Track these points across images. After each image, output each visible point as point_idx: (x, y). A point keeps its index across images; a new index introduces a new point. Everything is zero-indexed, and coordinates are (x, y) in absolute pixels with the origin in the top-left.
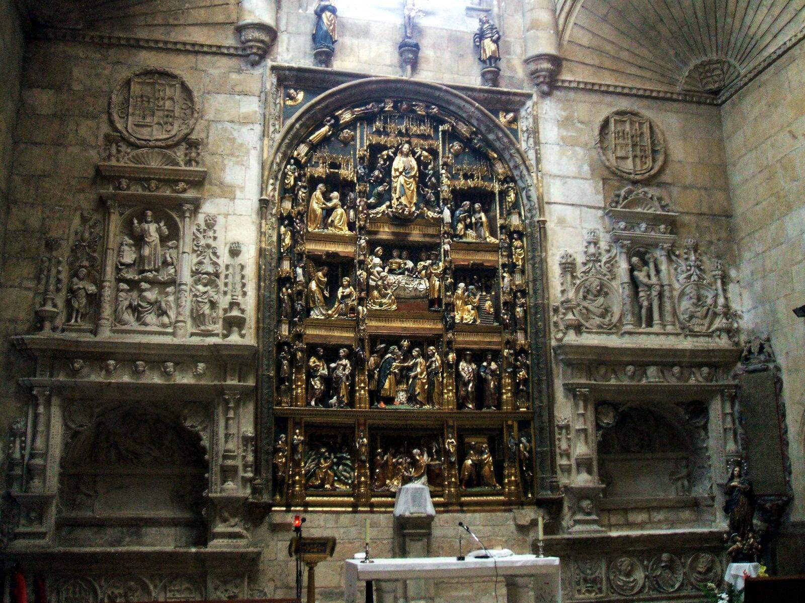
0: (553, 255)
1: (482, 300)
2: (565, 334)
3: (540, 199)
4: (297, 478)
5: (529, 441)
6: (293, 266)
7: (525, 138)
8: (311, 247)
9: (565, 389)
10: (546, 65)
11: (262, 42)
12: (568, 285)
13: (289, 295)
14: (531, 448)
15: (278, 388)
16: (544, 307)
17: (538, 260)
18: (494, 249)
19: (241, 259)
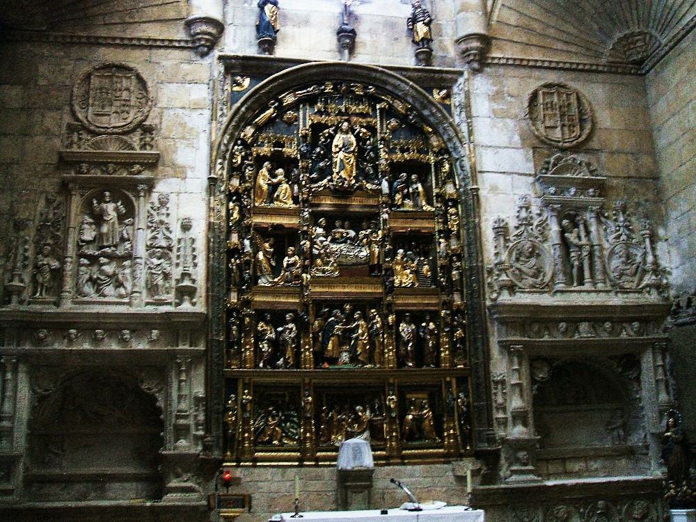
0: (487, 220)
1: (420, 264)
2: (499, 294)
3: (473, 168)
4: (246, 435)
5: (467, 396)
6: (241, 238)
7: (458, 113)
8: (257, 220)
9: (500, 346)
10: (475, 44)
11: (209, 34)
12: (501, 249)
13: (237, 265)
14: (469, 403)
15: (228, 352)
16: (478, 271)
17: (471, 225)
18: (430, 216)
19: (192, 233)
